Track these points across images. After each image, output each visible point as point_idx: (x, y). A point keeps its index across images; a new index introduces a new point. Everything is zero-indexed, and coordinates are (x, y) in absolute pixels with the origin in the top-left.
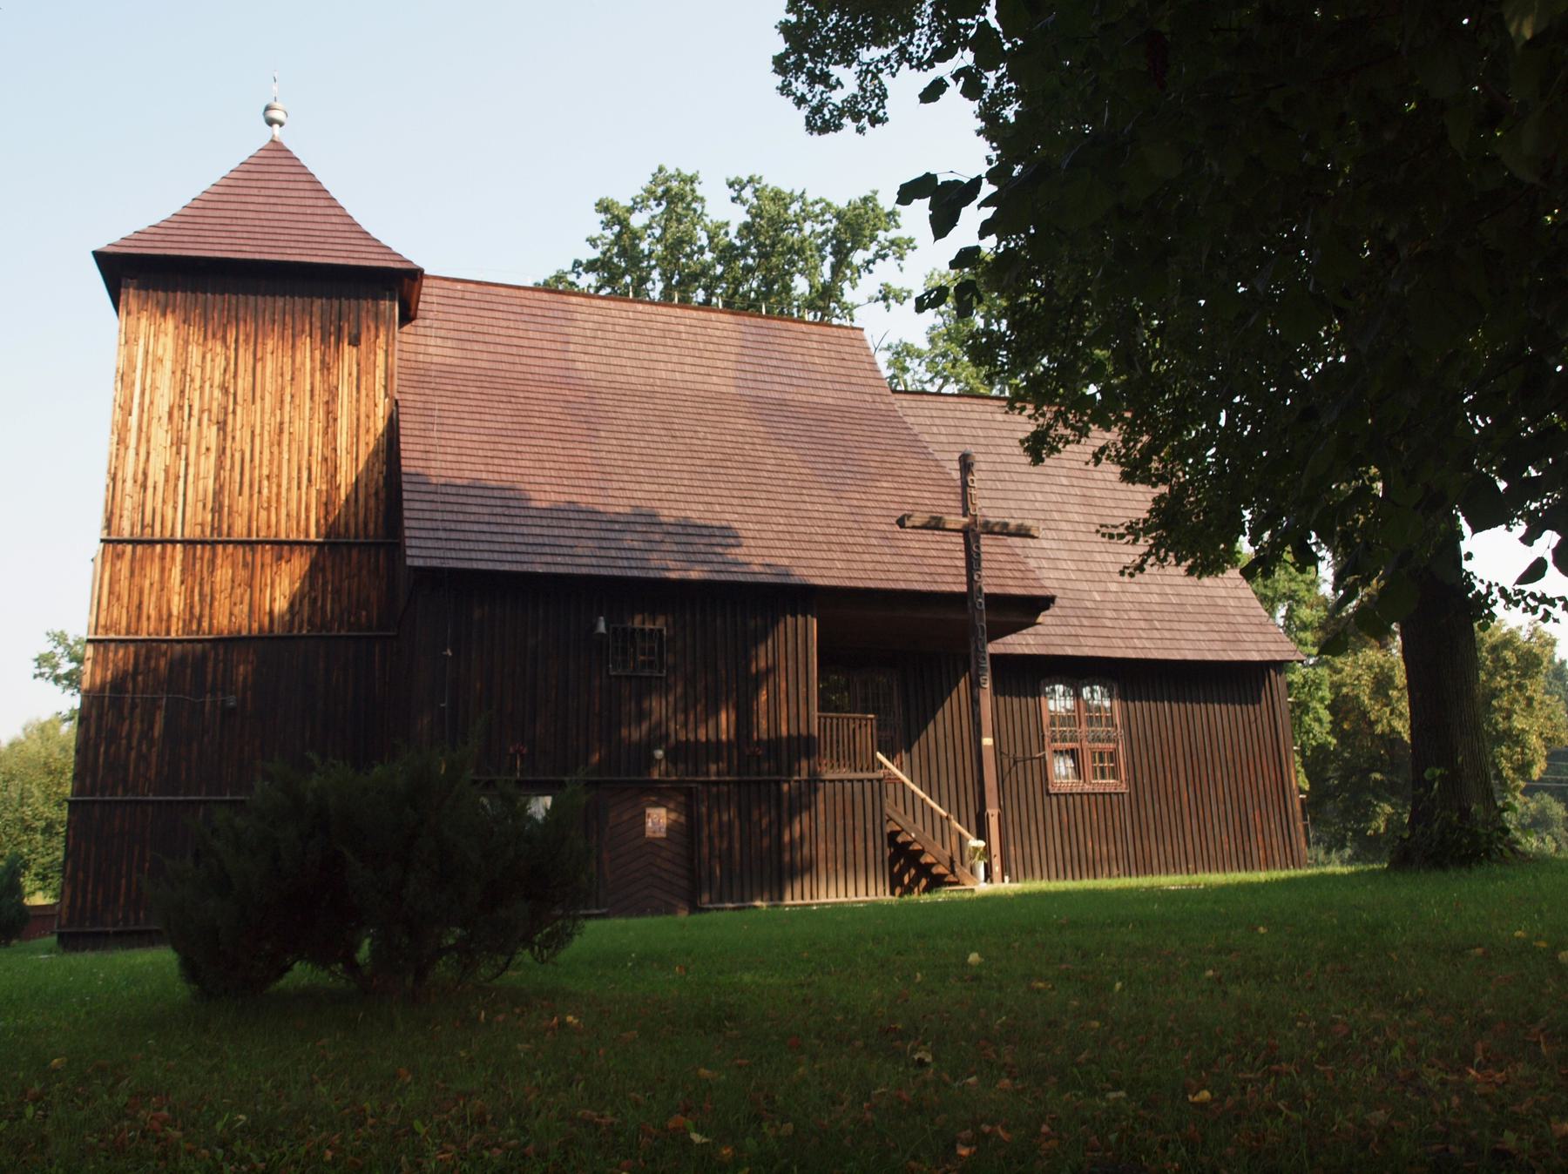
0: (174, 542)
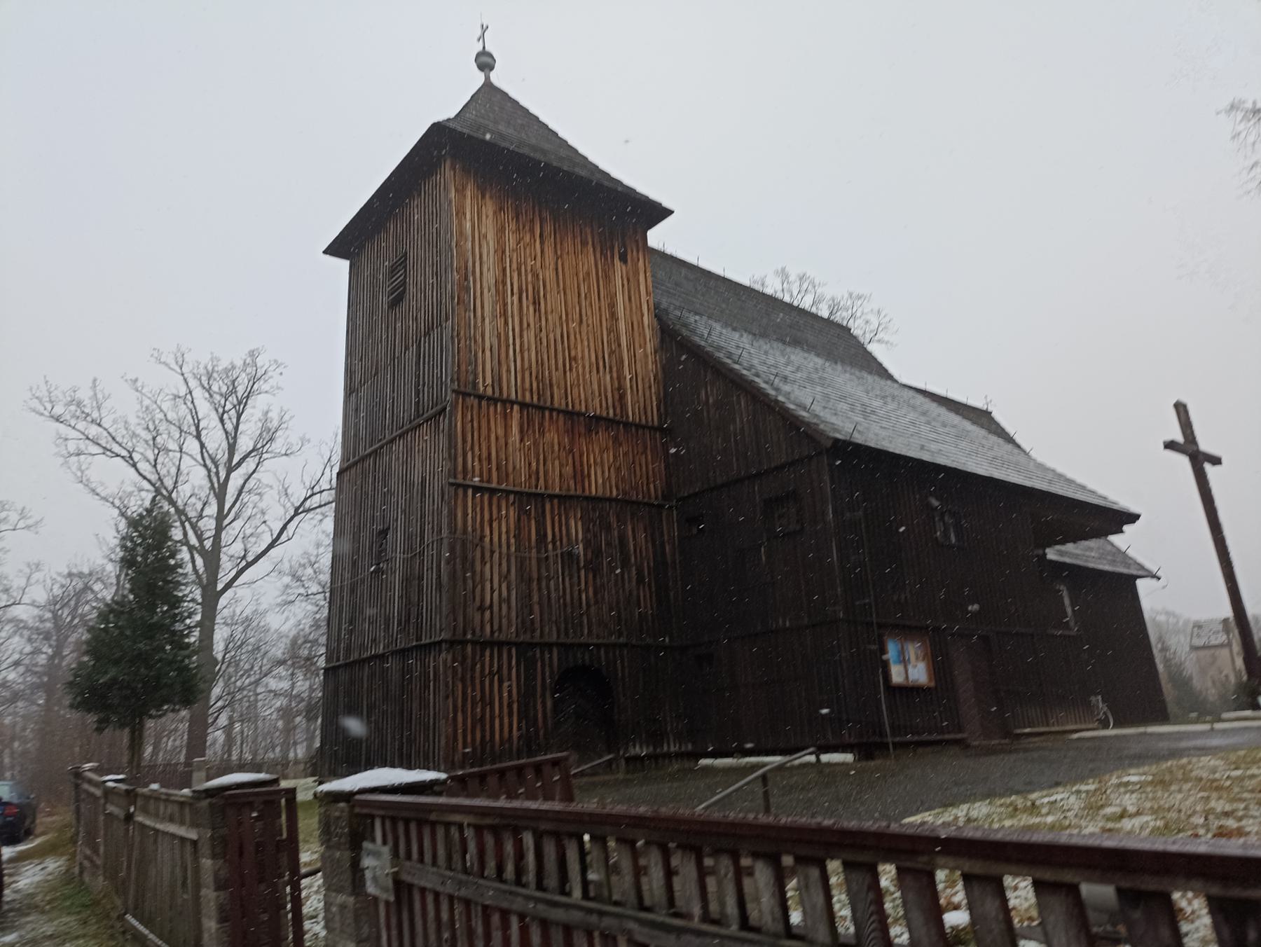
0: (512, 403)
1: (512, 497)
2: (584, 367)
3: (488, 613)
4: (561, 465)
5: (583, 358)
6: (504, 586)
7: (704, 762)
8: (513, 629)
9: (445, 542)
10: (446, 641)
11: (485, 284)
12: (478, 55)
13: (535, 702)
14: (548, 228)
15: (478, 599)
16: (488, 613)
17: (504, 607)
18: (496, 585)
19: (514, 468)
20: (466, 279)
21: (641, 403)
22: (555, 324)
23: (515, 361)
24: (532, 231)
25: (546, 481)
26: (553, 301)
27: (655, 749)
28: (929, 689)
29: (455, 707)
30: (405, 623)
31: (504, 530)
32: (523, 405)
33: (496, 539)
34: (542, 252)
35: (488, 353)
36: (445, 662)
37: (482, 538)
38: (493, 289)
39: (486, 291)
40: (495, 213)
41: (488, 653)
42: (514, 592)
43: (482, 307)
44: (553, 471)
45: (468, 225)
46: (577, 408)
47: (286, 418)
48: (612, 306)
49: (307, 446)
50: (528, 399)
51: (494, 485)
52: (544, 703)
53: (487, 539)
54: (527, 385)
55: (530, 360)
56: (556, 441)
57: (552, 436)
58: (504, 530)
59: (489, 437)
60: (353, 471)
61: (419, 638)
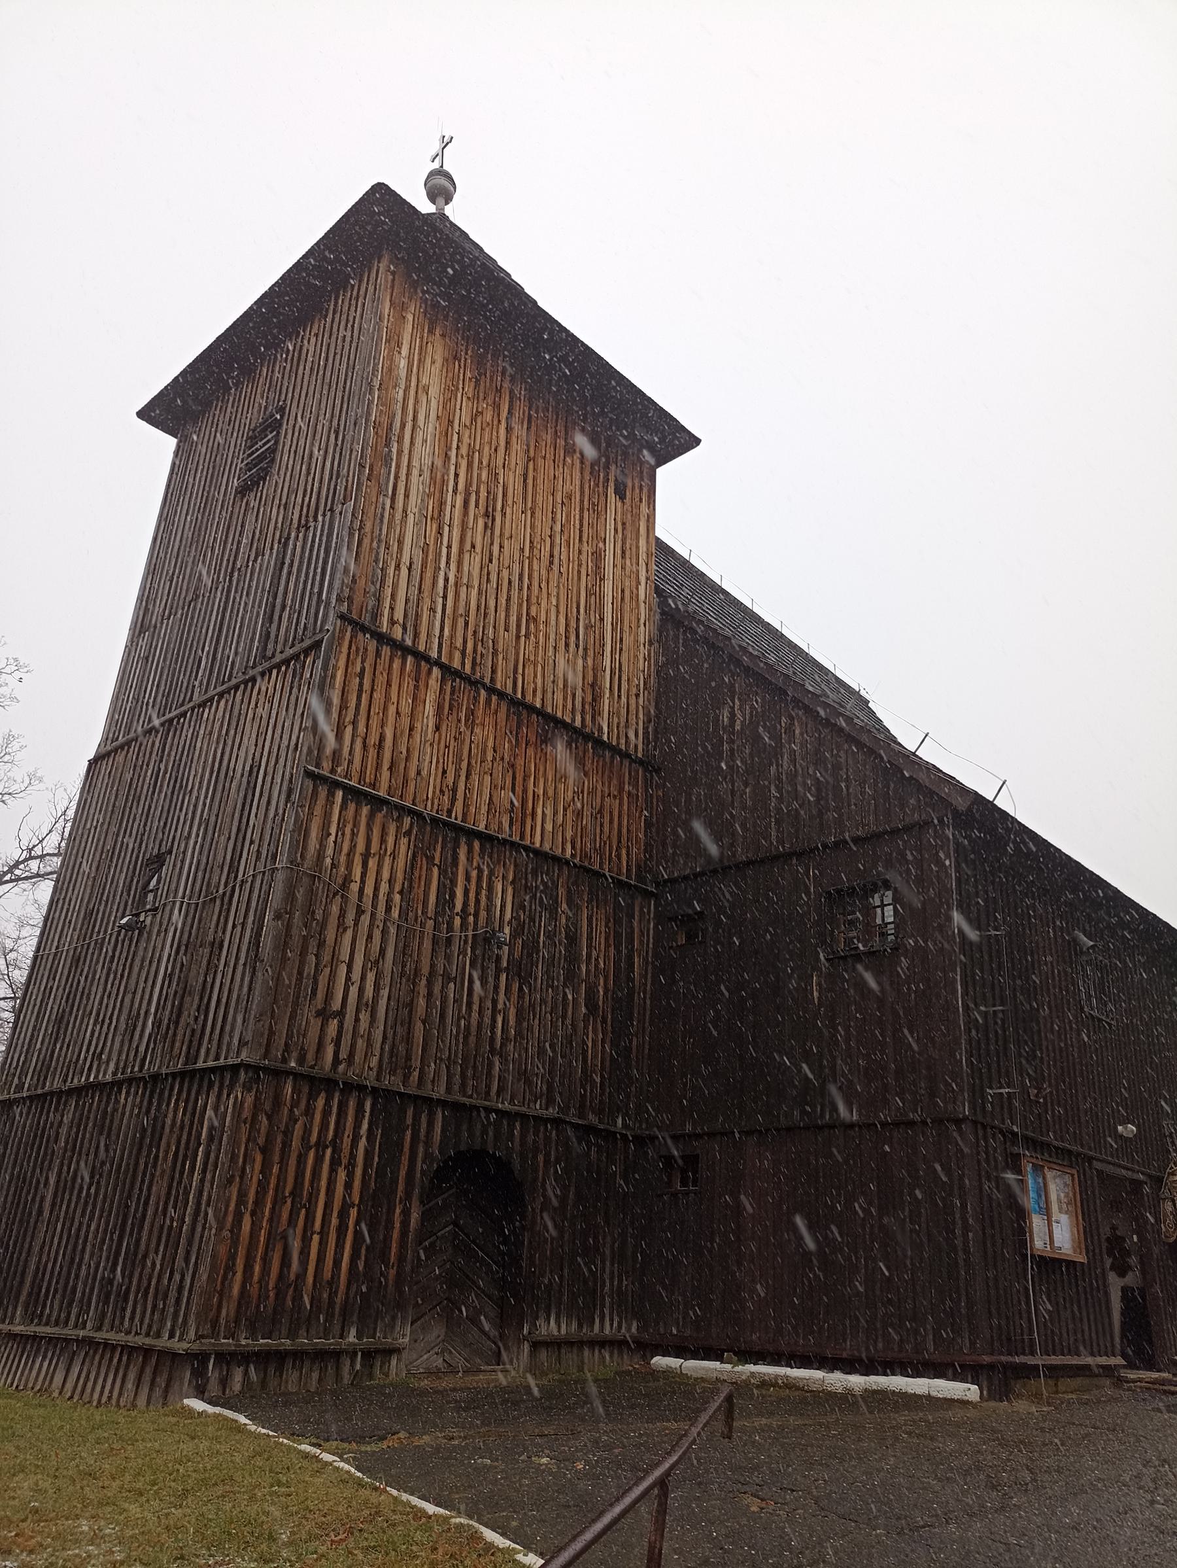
1: (407, 821)
2: (547, 637)
3: (334, 1024)
4: (494, 786)
5: (546, 623)
6: (371, 977)
7: (660, 1361)
8: (374, 1062)
9: (280, 876)
10: (248, 1067)
11: (415, 463)
12: (432, 174)
13: (390, 1211)
14: (520, 409)
15: (320, 995)
16: (334, 1024)
17: (364, 1017)
18: (356, 975)
19: (419, 773)
20: (388, 444)
21: (623, 718)
22: (511, 557)
23: (445, 597)
24: (497, 407)
25: (466, 805)
26: (514, 520)
27: (580, 1326)
28: (1071, 1264)
29: (242, 1200)
30: (164, 1033)
31: (386, 875)
32: (446, 669)
33: (369, 890)
34: (508, 443)
35: (404, 572)
36: (239, 1107)
37: (347, 880)
38: (427, 474)
39: (415, 472)
40: (446, 360)
41: (321, 1102)
42: (385, 993)
43: (407, 496)
44: (480, 793)
45: (403, 363)
46: (529, 698)
47: (15, 745)
48: (598, 556)
49: (37, 786)
50: (456, 664)
51: (382, 793)
52: (406, 1213)
53: (355, 887)
54: (459, 643)
55: (468, 603)
56: (490, 744)
57: (484, 734)
58: (386, 875)
59: (385, 709)
60: (120, 758)
61: (192, 1058)
